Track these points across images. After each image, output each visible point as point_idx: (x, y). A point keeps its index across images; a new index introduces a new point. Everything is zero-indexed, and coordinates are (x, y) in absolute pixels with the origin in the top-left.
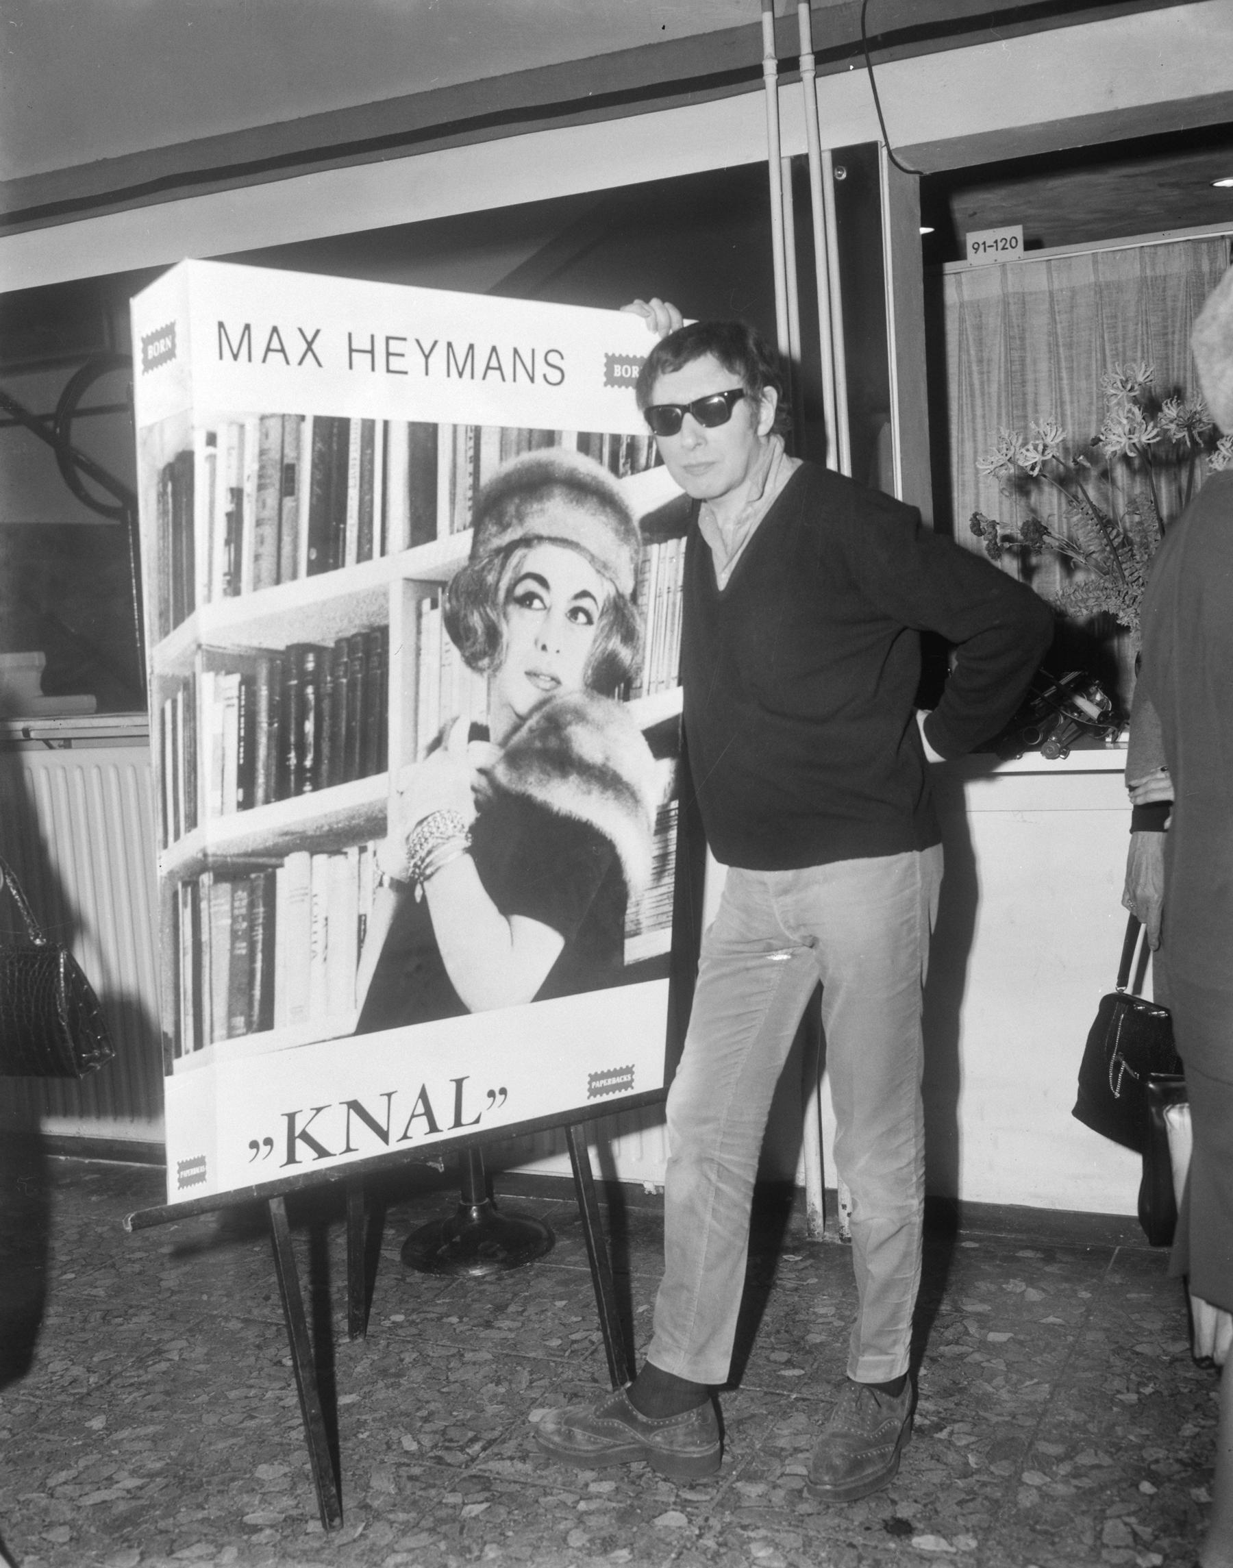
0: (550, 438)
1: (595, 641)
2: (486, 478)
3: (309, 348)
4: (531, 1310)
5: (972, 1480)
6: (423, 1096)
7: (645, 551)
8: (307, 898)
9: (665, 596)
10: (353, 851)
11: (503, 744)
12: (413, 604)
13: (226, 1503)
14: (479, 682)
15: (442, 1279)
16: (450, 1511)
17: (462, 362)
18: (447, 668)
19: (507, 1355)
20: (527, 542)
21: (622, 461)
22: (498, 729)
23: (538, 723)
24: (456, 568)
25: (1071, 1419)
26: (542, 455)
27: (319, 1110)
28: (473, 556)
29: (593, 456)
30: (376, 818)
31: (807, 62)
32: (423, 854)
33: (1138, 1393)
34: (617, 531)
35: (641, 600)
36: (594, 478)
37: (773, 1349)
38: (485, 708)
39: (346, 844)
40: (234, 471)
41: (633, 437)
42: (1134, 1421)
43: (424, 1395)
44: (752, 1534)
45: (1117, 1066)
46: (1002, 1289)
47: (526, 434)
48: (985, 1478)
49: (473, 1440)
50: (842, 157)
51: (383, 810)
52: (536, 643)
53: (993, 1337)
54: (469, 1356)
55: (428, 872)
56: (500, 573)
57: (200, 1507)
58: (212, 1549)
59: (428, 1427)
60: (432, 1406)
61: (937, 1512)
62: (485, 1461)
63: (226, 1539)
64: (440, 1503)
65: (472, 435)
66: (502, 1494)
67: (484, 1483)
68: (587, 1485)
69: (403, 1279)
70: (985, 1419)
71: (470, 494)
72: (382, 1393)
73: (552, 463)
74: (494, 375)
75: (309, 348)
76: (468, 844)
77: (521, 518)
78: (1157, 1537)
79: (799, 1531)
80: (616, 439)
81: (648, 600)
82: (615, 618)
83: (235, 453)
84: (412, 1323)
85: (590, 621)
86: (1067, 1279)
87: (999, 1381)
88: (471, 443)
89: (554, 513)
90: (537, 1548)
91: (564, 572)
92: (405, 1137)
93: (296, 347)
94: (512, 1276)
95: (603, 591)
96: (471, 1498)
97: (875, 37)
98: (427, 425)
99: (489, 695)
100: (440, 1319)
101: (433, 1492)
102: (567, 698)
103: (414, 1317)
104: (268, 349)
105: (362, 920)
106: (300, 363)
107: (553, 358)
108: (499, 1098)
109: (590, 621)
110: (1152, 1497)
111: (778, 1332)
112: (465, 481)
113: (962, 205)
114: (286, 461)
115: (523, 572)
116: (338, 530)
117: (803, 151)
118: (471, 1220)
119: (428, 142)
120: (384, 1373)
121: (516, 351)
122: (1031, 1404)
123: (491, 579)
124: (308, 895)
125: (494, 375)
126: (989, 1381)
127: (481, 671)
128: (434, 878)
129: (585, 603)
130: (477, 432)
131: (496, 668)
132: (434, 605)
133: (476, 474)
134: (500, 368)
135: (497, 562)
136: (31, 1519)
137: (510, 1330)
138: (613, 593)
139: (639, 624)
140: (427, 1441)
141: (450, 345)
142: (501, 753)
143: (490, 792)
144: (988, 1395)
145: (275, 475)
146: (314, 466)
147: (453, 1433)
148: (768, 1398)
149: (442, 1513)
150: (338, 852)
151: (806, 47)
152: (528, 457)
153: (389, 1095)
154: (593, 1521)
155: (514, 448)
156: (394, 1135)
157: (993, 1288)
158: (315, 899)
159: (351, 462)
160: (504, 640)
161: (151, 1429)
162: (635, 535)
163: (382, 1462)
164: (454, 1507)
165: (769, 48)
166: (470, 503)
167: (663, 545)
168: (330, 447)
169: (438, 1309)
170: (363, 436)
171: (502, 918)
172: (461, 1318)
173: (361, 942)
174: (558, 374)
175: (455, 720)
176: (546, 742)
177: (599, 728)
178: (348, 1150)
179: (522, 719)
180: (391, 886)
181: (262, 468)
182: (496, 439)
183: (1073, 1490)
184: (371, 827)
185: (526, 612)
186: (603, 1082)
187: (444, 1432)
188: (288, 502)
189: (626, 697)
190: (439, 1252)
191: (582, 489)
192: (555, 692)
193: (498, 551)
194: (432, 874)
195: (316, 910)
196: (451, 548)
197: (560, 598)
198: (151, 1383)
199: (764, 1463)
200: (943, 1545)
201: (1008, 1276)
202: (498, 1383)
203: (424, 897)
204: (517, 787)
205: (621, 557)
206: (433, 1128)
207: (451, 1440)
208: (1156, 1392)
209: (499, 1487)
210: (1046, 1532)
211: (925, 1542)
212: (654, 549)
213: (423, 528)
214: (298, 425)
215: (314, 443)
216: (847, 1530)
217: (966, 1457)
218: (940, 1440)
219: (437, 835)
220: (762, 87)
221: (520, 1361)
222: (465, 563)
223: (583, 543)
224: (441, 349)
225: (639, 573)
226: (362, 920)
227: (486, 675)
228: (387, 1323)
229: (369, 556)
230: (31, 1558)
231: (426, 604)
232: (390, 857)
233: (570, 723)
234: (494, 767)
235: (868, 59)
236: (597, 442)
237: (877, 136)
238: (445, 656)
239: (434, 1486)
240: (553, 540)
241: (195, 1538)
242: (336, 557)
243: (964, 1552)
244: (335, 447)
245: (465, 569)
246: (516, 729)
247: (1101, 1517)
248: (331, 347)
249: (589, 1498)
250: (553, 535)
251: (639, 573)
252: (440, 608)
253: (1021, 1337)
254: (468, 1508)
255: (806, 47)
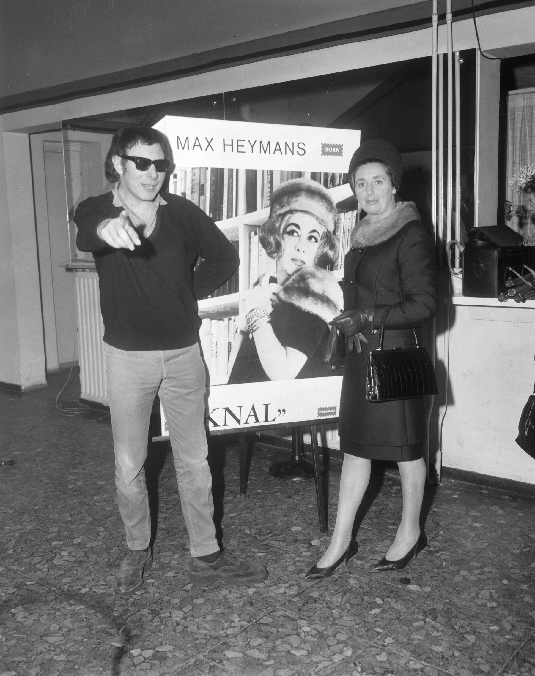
0: (300, 174)
1: (319, 248)
2: (275, 189)
3: (209, 144)
4: (307, 495)
5: (440, 570)
6: (253, 409)
7: (339, 216)
8: (210, 335)
9: (347, 232)
10: (226, 319)
11: (283, 284)
12: (247, 234)
13: (181, 541)
14: (273, 262)
15: (280, 480)
16: (252, 554)
17: (266, 148)
18: (261, 256)
19: (292, 508)
20: (291, 212)
21: (329, 183)
22: (281, 278)
23: (296, 277)
24: (264, 221)
25: (489, 556)
26: (297, 180)
27: (214, 409)
28: (270, 217)
29: (317, 181)
30: (234, 308)
31: (449, 16)
32: (252, 322)
33: (521, 550)
34: (327, 208)
35: (337, 234)
36: (318, 189)
37: (389, 518)
38: (275, 271)
39: (224, 317)
40: (183, 187)
41: (333, 174)
42: (514, 560)
43: (258, 517)
44: (351, 576)
45: (528, 423)
46: (489, 509)
47: (290, 173)
48: (446, 570)
49: (269, 533)
50: (463, 54)
51: (237, 306)
52: (295, 248)
53: (475, 524)
54: (279, 506)
55: (254, 329)
56: (281, 223)
57: (173, 541)
58: (172, 554)
59: (256, 527)
60: (260, 521)
61: (422, 578)
62: (271, 540)
63: (177, 551)
64: (250, 551)
65: (269, 174)
66: (272, 551)
67: (267, 547)
68: (302, 552)
69: (267, 479)
70: (457, 551)
71: (269, 194)
72: (245, 514)
73: (301, 184)
74: (278, 152)
75: (209, 144)
76: (269, 320)
77: (289, 203)
78: (499, 598)
79: (369, 577)
80: (326, 175)
81: (340, 233)
82: (327, 240)
83: (183, 181)
84: (264, 493)
85: (316, 241)
86: (516, 508)
87: (470, 540)
88: (269, 177)
89: (302, 202)
90: (276, 569)
91: (306, 224)
92: (246, 423)
93: (204, 144)
94: (306, 482)
95: (321, 230)
96: (261, 551)
97: (477, 6)
98: (253, 170)
99: (277, 266)
100: (274, 493)
101: (249, 547)
102: (307, 269)
103: (265, 491)
104: (195, 145)
105: (230, 344)
106: (206, 150)
107: (301, 146)
108: (283, 413)
109: (316, 241)
110: (505, 585)
111: (394, 513)
112: (267, 190)
113: (520, 73)
114: (201, 183)
115: (290, 223)
116: (220, 207)
117: (446, 52)
118: (295, 460)
119: (359, 38)
120: (248, 508)
121: (286, 143)
122: (477, 548)
123: (277, 225)
124: (210, 334)
125: (278, 152)
126: (465, 539)
127: (274, 258)
128: (257, 331)
129: (315, 234)
130: (272, 173)
131: (280, 257)
132: (256, 234)
133: (271, 187)
134: (280, 150)
135: (280, 219)
136: (119, 537)
137: (297, 500)
138: (326, 231)
139: (336, 242)
140: (253, 531)
141: (261, 142)
142: (282, 288)
143: (277, 301)
144: (462, 544)
145: (197, 188)
146: (211, 185)
147: (264, 530)
148: (379, 534)
149: (249, 554)
150: (221, 319)
151: (449, 10)
152: (291, 181)
153: (240, 407)
154: (299, 564)
155: (286, 178)
156: (243, 421)
157: (485, 508)
158: (212, 336)
159: (225, 184)
160: (283, 247)
161: (165, 515)
162: (334, 210)
163: (236, 536)
164: (254, 553)
165: (435, 11)
166: (269, 198)
167: (346, 214)
168: (217, 179)
169: (275, 490)
170: (229, 175)
171: (283, 348)
172: (281, 494)
173: (229, 352)
174: (303, 151)
175: (264, 275)
176: (299, 284)
177: (321, 280)
178: (225, 425)
179: (290, 276)
180: (240, 333)
181: (193, 186)
182: (279, 175)
183: (477, 579)
184: (233, 312)
185: (291, 237)
186: (324, 411)
187: (260, 530)
188: (202, 198)
189: (331, 269)
190: (281, 470)
191: (312, 193)
192: (303, 266)
193: (280, 215)
194: (256, 330)
195: (213, 339)
196: (262, 214)
197: (304, 232)
198: (171, 501)
199: (368, 554)
200: (419, 589)
201: (493, 504)
202: (285, 517)
203: (253, 338)
204: (289, 301)
205: (329, 218)
206: (257, 421)
207: (262, 532)
208: (529, 551)
209: (272, 549)
210: (459, 590)
211: (412, 587)
212: (342, 215)
213: (251, 207)
214: (206, 171)
215: (211, 178)
216: (386, 579)
217: (442, 563)
218: (436, 556)
219: (257, 316)
220: (432, 26)
221: (296, 510)
222: (267, 219)
223: (313, 213)
224: (258, 144)
225: (336, 224)
226: (230, 344)
227: (275, 259)
228: (255, 492)
229: (232, 216)
230: (116, 548)
231: (253, 233)
232: (240, 322)
233: (309, 278)
234: (279, 292)
235: (474, 15)
236: (319, 176)
237: (477, 46)
238: (260, 252)
239: (250, 545)
240: (301, 211)
241: (168, 550)
242: (219, 217)
243: (425, 592)
244: (219, 178)
245: (267, 221)
246: (287, 279)
247: (481, 589)
248: (217, 144)
249: (301, 557)
250: (302, 209)
251: (336, 224)
252: (258, 235)
253: (487, 526)
254: (258, 554)
255: (449, 10)
